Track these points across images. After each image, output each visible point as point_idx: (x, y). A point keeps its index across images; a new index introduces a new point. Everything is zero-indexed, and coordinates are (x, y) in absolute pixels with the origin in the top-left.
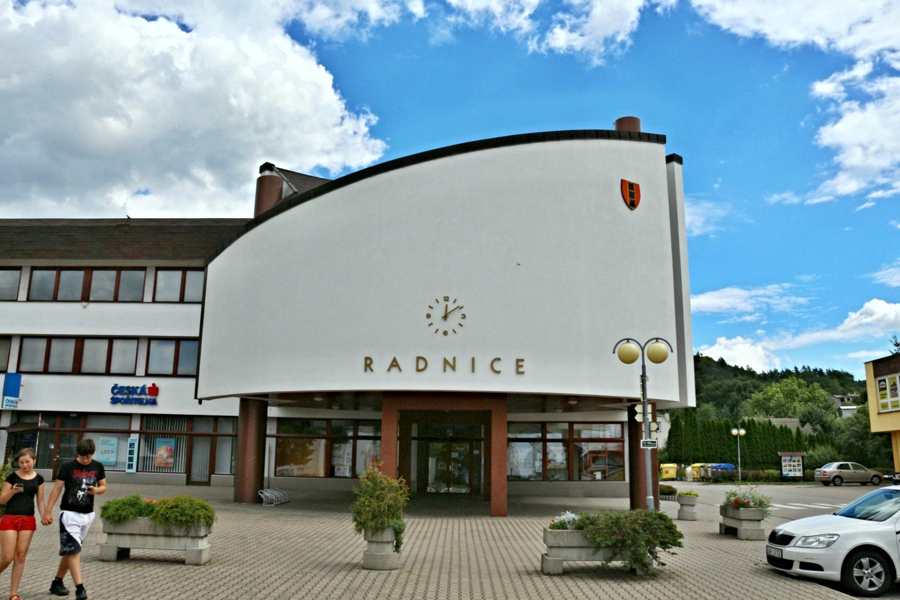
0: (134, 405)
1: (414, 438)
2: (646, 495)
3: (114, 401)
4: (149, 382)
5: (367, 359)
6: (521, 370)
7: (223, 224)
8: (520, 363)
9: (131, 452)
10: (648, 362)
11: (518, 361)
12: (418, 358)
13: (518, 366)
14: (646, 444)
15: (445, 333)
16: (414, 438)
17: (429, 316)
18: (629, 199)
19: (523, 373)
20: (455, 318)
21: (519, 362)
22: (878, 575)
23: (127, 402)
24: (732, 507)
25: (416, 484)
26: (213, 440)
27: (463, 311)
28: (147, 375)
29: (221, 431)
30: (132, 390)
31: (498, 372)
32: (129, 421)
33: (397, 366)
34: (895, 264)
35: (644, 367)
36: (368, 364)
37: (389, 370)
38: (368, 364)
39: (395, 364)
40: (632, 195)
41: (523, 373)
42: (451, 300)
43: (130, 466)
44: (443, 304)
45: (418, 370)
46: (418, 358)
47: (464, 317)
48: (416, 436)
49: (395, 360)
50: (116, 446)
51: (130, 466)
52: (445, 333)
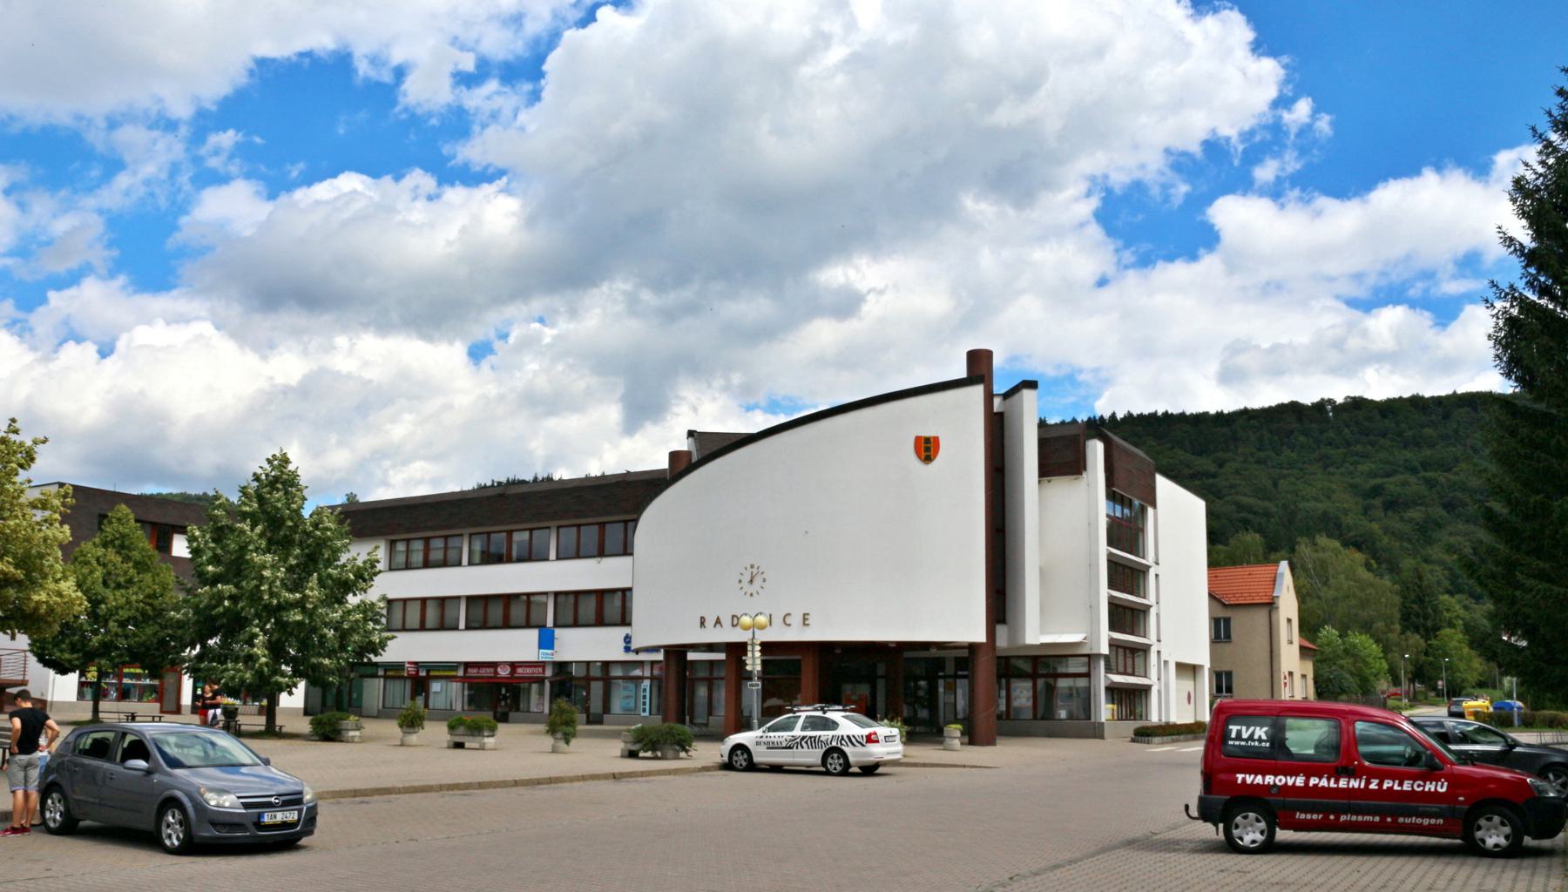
2: (753, 719)
5: (702, 618)
6: (807, 622)
8: (806, 617)
10: (756, 630)
11: (804, 615)
12: (733, 616)
13: (805, 619)
14: (757, 685)
15: (751, 595)
17: (740, 581)
19: (808, 625)
20: (758, 581)
21: (805, 617)
22: (840, 765)
26: (710, 682)
27: (764, 576)
29: (715, 674)
31: (789, 625)
32: (1267, 615)
33: (720, 623)
35: (754, 633)
36: (702, 622)
38: (702, 622)
39: (718, 622)
41: (808, 625)
42: (756, 567)
43: (644, 710)
44: (750, 570)
45: (733, 626)
47: (764, 580)
48: (884, 674)
49: (718, 618)
50: (634, 692)
51: (644, 710)
52: (751, 595)
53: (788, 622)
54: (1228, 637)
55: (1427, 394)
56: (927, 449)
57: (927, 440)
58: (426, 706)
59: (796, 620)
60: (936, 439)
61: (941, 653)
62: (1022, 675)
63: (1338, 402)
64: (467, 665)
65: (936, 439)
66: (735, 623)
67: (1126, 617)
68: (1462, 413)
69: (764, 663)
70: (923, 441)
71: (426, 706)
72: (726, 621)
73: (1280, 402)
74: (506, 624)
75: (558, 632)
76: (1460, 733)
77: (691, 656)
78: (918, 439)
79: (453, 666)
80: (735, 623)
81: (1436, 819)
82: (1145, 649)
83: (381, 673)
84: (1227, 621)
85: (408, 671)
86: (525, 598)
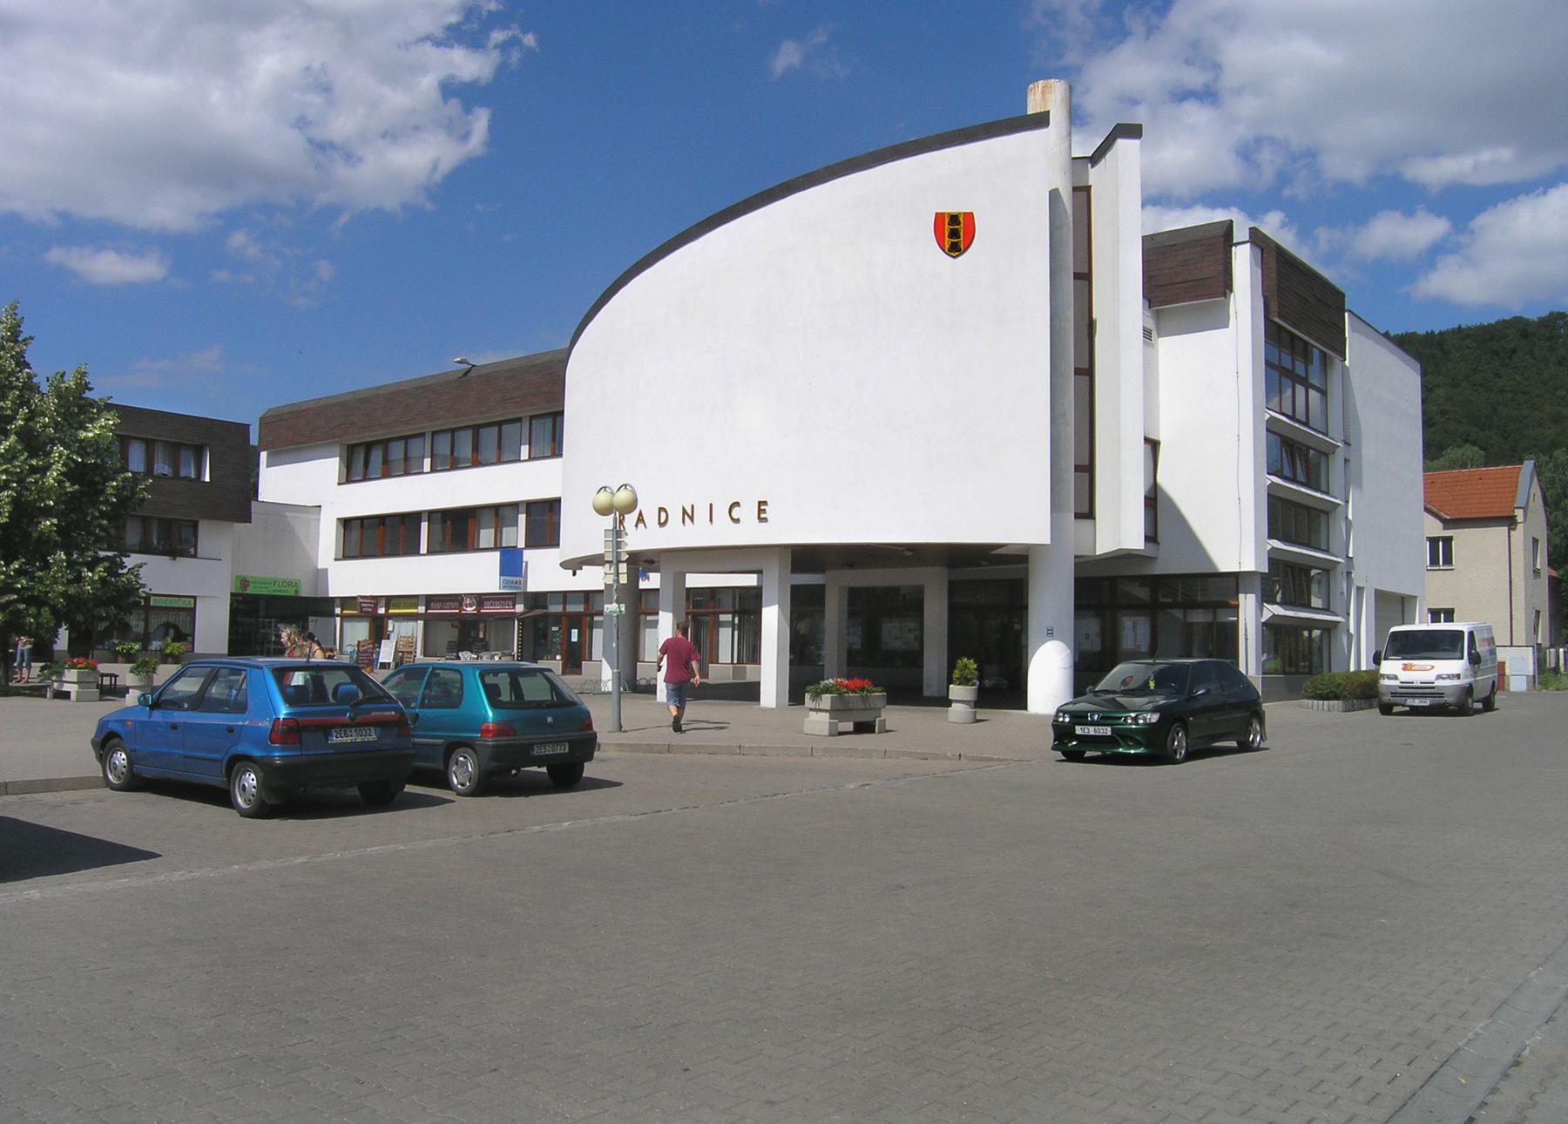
0: (1533, 316)
1: (564, 608)
7: (959, 142)
11: (760, 503)
13: (760, 511)
16: (564, 608)
19: (765, 520)
31: (737, 521)
34: (444, 746)
37: (636, 526)
41: (765, 520)
46: (661, 509)
48: (562, 607)
53: (735, 517)
54: (1448, 560)
55: (1455, 615)
57: (954, 219)
59: (748, 512)
60: (969, 217)
62: (1136, 607)
64: (430, 600)
65: (969, 217)
66: (663, 520)
70: (947, 220)
72: (675, 516)
73: (1501, 318)
76: (123, 586)
78: (939, 217)
79: (412, 600)
80: (663, 520)
82: (1328, 569)
84: (1448, 541)
85: (362, 608)
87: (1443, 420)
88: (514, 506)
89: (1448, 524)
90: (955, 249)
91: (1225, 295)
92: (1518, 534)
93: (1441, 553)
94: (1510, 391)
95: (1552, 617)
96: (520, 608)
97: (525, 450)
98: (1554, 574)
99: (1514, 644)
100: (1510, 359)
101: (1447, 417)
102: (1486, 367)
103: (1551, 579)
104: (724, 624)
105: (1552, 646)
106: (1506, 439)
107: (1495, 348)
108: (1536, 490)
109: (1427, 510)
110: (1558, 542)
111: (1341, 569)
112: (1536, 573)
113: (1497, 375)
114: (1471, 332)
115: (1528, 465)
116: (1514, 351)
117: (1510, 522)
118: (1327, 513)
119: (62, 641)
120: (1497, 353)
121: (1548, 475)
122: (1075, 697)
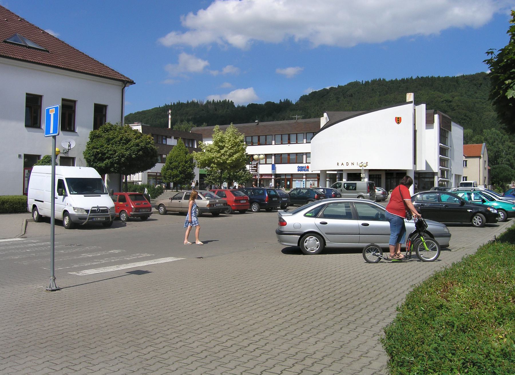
3: (299, 170)
4: (306, 165)
9: (304, 184)
18: (397, 122)
23: (301, 170)
24: (466, 180)
25: (50, 236)
28: (306, 163)
30: (302, 167)
39: (342, 164)
40: (398, 120)
56: (398, 120)
57: (398, 118)
58: (141, 181)
61: (393, 172)
63: (294, 102)
65: (401, 118)
67: (442, 162)
68: (380, 102)
69: (434, 178)
71: (141, 181)
73: (477, 73)
74: (289, 162)
75: (276, 165)
77: (327, 172)
78: (396, 118)
81: (88, 265)
83: (304, 177)
84: (466, 161)
86: (287, 156)
87: (457, 108)
88: (271, 155)
89: (466, 157)
90: (398, 123)
91: (433, 124)
92: (481, 160)
93: (465, 164)
94: (480, 98)
95: (489, 178)
96: (273, 177)
97: (273, 142)
98: (489, 168)
99: (265, 136)
100: (480, 87)
101: (459, 107)
102: (472, 90)
103: (489, 170)
104: (327, 181)
105: (488, 185)
106: (478, 115)
107: (475, 83)
108: (486, 150)
109: (464, 155)
110: (492, 155)
111: (450, 171)
112: (485, 168)
113: (476, 93)
114: (467, 77)
115: (484, 144)
116: (481, 84)
117: (480, 157)
118: (447, 160)
119: (172, 185)
120: (476, 85)
121: (490, 136)
122: (414, 193)
